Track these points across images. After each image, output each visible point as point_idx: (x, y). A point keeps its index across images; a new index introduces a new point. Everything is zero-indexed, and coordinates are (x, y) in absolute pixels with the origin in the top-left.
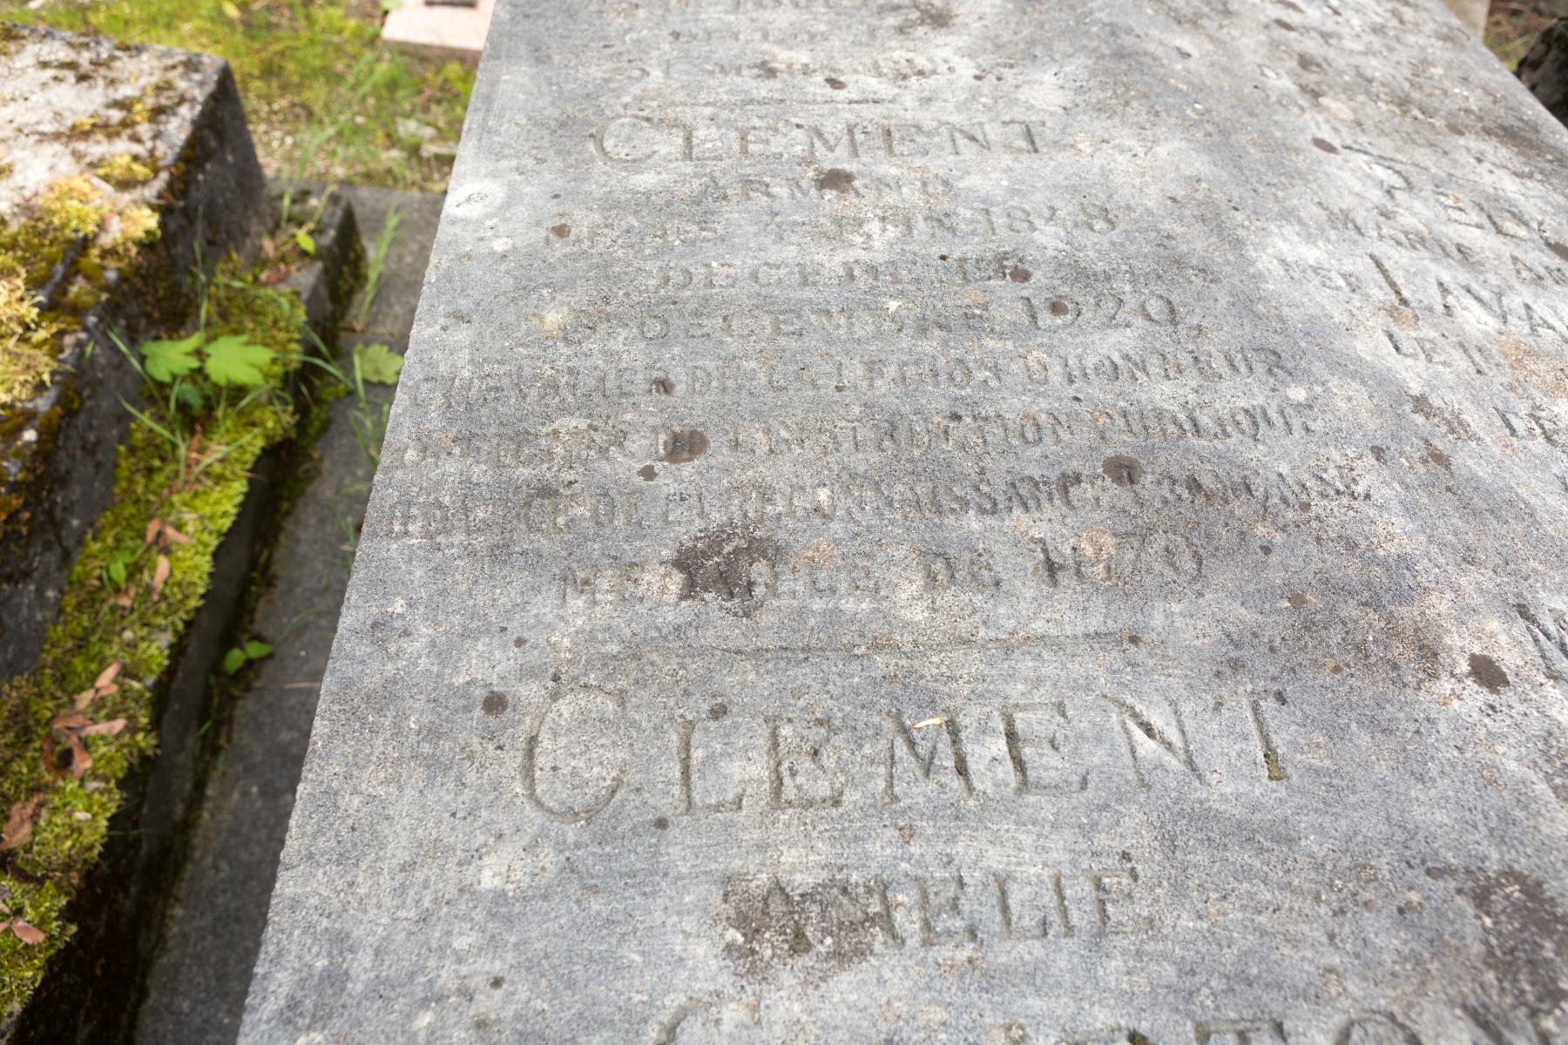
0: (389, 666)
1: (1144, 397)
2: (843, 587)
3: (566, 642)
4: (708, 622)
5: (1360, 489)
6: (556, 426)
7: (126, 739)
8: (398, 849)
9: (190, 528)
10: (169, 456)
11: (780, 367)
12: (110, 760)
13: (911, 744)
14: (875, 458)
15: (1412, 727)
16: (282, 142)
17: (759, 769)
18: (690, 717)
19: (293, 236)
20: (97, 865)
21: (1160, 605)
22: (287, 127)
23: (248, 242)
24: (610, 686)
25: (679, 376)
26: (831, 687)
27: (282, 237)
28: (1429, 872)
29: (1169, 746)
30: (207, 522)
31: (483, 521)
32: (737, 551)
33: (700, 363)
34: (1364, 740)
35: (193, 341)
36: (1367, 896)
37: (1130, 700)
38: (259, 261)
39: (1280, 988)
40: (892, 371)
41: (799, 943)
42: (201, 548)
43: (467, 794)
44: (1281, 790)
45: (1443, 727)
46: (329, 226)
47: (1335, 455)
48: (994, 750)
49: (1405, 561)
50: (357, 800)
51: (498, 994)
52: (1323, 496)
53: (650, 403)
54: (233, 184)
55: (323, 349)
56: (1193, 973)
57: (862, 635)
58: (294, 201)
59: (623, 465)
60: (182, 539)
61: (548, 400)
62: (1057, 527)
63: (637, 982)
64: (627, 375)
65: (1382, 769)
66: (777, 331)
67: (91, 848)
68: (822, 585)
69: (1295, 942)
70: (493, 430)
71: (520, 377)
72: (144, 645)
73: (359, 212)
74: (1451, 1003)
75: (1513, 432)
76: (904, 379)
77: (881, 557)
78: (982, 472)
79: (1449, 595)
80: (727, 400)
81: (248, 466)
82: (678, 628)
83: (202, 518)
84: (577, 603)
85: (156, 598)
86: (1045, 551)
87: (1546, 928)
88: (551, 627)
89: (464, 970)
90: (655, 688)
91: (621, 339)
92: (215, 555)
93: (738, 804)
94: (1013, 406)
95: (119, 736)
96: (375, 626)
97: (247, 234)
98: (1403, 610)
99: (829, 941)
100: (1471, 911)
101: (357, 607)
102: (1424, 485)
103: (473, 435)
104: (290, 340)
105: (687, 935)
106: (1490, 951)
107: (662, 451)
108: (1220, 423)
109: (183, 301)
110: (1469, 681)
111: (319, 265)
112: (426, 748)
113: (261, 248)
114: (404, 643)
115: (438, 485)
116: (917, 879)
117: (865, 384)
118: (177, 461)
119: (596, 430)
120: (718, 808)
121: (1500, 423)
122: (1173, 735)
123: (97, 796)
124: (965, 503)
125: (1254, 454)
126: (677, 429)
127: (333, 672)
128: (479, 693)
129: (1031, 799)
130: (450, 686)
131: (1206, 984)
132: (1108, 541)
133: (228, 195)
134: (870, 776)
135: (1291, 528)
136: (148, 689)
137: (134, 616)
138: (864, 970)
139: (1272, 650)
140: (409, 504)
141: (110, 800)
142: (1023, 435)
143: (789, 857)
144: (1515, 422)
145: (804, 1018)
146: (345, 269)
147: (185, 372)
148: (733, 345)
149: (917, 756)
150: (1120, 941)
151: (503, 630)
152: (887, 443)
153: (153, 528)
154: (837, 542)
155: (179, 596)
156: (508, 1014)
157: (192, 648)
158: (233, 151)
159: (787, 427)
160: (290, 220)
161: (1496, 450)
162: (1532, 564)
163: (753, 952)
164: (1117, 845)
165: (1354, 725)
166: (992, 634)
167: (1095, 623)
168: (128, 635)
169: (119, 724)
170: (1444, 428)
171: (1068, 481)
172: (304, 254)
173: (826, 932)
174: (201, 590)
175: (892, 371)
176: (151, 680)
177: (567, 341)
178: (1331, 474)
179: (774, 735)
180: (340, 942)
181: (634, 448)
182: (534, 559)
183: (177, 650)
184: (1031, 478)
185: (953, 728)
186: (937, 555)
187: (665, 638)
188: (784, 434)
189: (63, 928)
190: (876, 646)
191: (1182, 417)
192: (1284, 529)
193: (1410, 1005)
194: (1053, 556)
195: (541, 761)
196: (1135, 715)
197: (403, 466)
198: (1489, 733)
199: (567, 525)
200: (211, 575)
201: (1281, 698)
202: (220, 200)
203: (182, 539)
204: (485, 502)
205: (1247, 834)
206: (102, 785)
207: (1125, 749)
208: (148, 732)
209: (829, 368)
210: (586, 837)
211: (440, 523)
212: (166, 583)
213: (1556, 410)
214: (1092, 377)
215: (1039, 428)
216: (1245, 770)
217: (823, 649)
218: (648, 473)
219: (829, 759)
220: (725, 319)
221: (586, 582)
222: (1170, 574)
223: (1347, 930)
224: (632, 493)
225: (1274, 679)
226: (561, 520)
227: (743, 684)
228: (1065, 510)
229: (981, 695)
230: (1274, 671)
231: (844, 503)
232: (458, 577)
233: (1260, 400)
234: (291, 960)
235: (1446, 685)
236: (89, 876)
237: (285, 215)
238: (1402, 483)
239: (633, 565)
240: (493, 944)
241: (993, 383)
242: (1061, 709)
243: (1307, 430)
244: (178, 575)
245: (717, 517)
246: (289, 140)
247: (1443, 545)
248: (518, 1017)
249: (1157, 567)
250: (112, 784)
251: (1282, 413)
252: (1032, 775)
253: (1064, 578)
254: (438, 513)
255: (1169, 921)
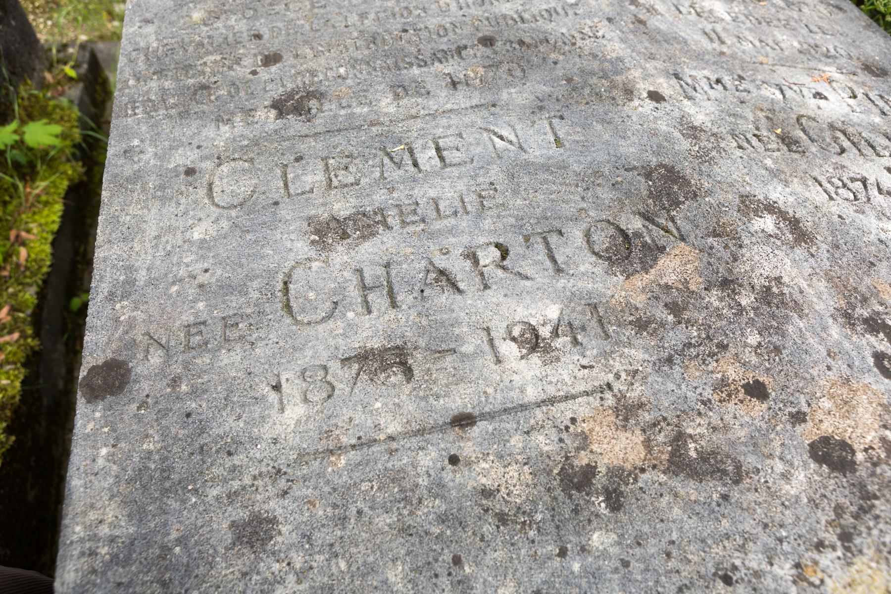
0: (135, 166)
1: (497, 11)
2: (354, 104)
3: (222, 144)
4: (290, 126)
5: (600, 34)
6: (205, 60)
7: (22, 342)
8: (151, 230)
9: (35, 231)
10: (14, 194)
11: (316, 21)
12: (15, 354)
13: (391, 158)
14: (366, 52)
15: (621, 120)
16: (45, 26)
17: (320, 177)
18: (285, 163)
19: (63, 70)
20: (19, 407)
21: (505, 91)
22: (46, 16)
23: (36, 74)
24: (246, 157)
25: (266, 33)
26: (352, 142)
27: (56, 71)
28: (626, 170)
29: (511, 142)
30: (44, 227)
31: (173, 104)
32: (302, 97)
33: (275, 25)
34: (599, 127)
35: (14, 125)
36: (598, 182)
37: (492, 128)
38: (43, 85)
39: (560, 218)
40: (372, 16)
41: (345, 236)
42: (43, 241)
43: (182, 207)
44: (562, 150)
45: (634, 118)
46: (83, 62)
47: (589, 22)
48: (430, 154)
49: (620, 59)
50: (128, 218)
51: (207, 275)
52: (583, 39)
53: (252, 46)
54: (18, 39)
55: (93, 125)
56: (522, 219)
57: (365, 121)
58: (58, 51)
59: (241, 72)
60: (31, 237)
61: (199, 50)
62: (456, 67)
63: (271, 260)
64: (238, 35)
65: (606, 137)
66: (313, 7)
67: (13, 397)
68: (344, 105)
69: (566, 202)
70: (173, 66)
71: (183, 42)
72: (21, 294)
73: (100, 56)
74: (634, 213)
75: (680, 12)
76: (378, 19)
77: (372, 90)
78: (419, 50)
79: (640, 70)
80: (290, 38)
81: (62, 195)
82: (276, 131)
83: (40, 225)
84: (225, 128)
85: (22, 269)
86: (451, 78)
87: (675, 182)
88: (214, 139)
89: (190, 269)
90: (267, 155)
91: (233, 20)
92: (53, 244)
93: (311, 191)
94: (433, 22)
95: (17, 341)
96: (125, 152)
97: (34, 70)
98: (618, 78)
99: (358, 232)
100: (643, 180)
101: (115, 146)
102: (632, 32)
103: (163, 70)
104: (73, 127)
105: (292, 240)
106: (651, 192)
107: (260, 63)
108: (534, 17)
109: (3, 107)
110: (647, 100)
111: (81, 85)
112: (159, 193)
113: (44, 78)
114: (141, 156)
115: (148, 92)
116: (397, 206)
117: (359, 23)
118: (19, 197)
119: (225, 59)
120: (303, 193)
121: (673, 9)
122: (512, 138)
123: (11, 372)
124: (411, 65)
125: (550, 27)
126: (267, 53)
127: (108, 172)
128: (182, 169)
129: (448, 170)
130: (167, 169)
131: (528, 222)
132: (481, 71)
133: (17, 45)
134: (372, 172)
135: (568, 53)
136: (30, 316)
137: (13, 280)
138: (376, 240)
139: (558, 100)
140: (135, 102)
141: (20, 373)
142: (438, 34)
143: (337, 206)
144: (681, 9)
145: (349, 261)
146: (98, 88)
147: (13, 143)
148: (291, 15)
149: (394, 163)
150: (489, 213)
151: (190, 144)
152: (372, 45)
153: (13, 234)
154: (350, 87)
155: (36, 267)
156: (214, 280)
157: (50, 296)
158: (14, 18)
159: (322, 46)
160: (58, 62)
161: (671, 19)
162: (683, 59)
163: (324, 242)
164: (488, 180)
165: (594, 123)
166: (427, 112)
167: (475, 102)
168: (11, 290)
169: (16, 335)
170: (645, 11)
171: (460, 50)
172: (71, 79)
173: (356, 230)
174: (48, 263)
175: (372, 16)
176: (29, 311)
177: (205, 25)
178: (587, 30)
179: (327, 165)
180: (130, 269)
181: (245, 64)
182: (201, 115)
183: (41, 295)
184: (443, 50)
185: (411, 151)
186: (399, 86)
187: (270, 135)
188: (320, 48)
189: (7, 439)
190: (372, 124)
191: (515, 16)
192: (564, 54)
193: (616, 216)
194: (455, 79)
195: (215, 189)
196: (495, 134)
197: (128, 87)
198: (655, 117)
199: (216, 99)
200: (52, 254)
201: (562, 118)
202: (13, 48)
203: (31, 237)
204: (173, 96)
205: (546, 168)
206: (13, 367)
207: (490, 147)
208: (33, 338)
209: (340, 18)
210: (241, 213)
211: (151, 107)
212: (27, 260)
213: (703, 4)
214: (472, 6)
215: (446, 29)
216: (545, 146)
217: (346, 129)
218: (254, 73)
219: (353, 169)
220: (286, 5)
221: (229, 120)
222: (510, 78)
223: (590, 194)
224: (247, 82)
225: (558, 111)
226: (213, 98)
227: (310, 147)
228: (459, 60)
229: (423, 135)
230: (558, 108)
231: (351, 73)
232: (164, 127)
233: (553, 5)
234: (108, 279)
235: (636, 102)
236: (16, 411)
237: (55, 58)
238: (620, 31)
239: (251, 110)
240: (203, 258)
241: (423, 14)
242: (460, 135)
243: (576, 14)
244: (33, 256)
245: (290, 86)
246: (49, 23)
247: (639, 53)
248: (218, 281)
249: (504, 76)
250: (19, 365)
251: (564, 9)
252: (447, 161)
253: (459, 87)
254: (150, 104)
255: (511, 203)
